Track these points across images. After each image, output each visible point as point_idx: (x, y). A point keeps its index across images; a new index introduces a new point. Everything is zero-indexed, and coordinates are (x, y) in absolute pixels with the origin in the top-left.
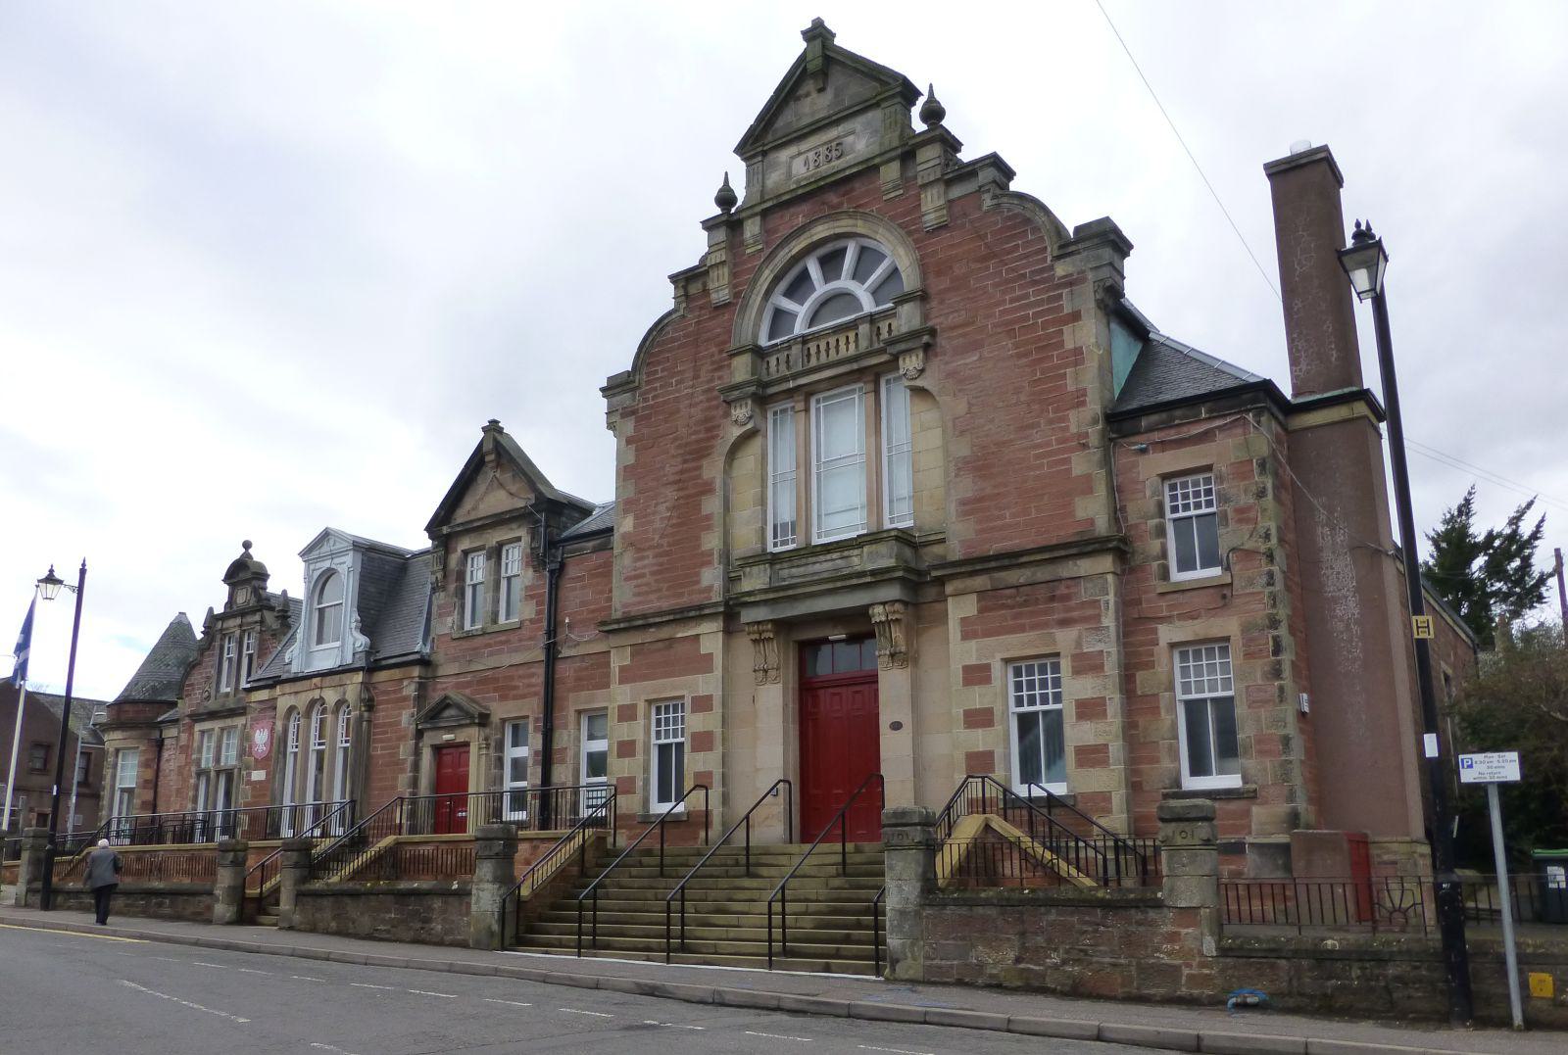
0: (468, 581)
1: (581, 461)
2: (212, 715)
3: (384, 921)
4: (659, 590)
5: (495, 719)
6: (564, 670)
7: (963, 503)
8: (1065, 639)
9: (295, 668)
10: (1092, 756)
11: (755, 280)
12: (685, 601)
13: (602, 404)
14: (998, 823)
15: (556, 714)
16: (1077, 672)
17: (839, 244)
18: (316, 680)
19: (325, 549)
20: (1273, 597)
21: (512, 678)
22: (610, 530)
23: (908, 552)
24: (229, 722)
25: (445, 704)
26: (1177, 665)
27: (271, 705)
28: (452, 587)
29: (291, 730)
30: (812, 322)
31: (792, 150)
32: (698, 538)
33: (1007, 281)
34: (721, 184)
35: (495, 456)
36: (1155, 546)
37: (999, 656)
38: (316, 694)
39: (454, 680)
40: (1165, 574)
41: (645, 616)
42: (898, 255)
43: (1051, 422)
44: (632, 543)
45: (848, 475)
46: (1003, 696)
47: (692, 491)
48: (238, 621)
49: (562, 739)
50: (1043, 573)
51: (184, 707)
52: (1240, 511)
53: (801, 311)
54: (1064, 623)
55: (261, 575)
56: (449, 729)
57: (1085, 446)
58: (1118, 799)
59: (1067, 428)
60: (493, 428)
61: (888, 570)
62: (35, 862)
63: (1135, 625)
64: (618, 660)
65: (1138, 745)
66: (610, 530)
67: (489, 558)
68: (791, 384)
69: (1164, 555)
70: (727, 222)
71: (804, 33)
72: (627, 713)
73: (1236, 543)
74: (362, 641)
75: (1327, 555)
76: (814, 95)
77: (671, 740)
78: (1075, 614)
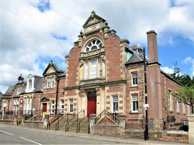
0: (48, 81)
1: (63, 66)
4: (71, 84)
8: (119, 93)
10: (121, 108)
12: (73, 86)
14: (107, 116)
27: (23, 97)
32: (76, 78)
38: (28, 96)
40: (131, 85)
45: (91, 71)
46: (112, 100)
51: (13, 96)
53: (90, 48)
54: (119, 91)
63: (128, 91)
64: (66, 93)
65: (128, 107)
69: (131, 82)
78: (120, 90)
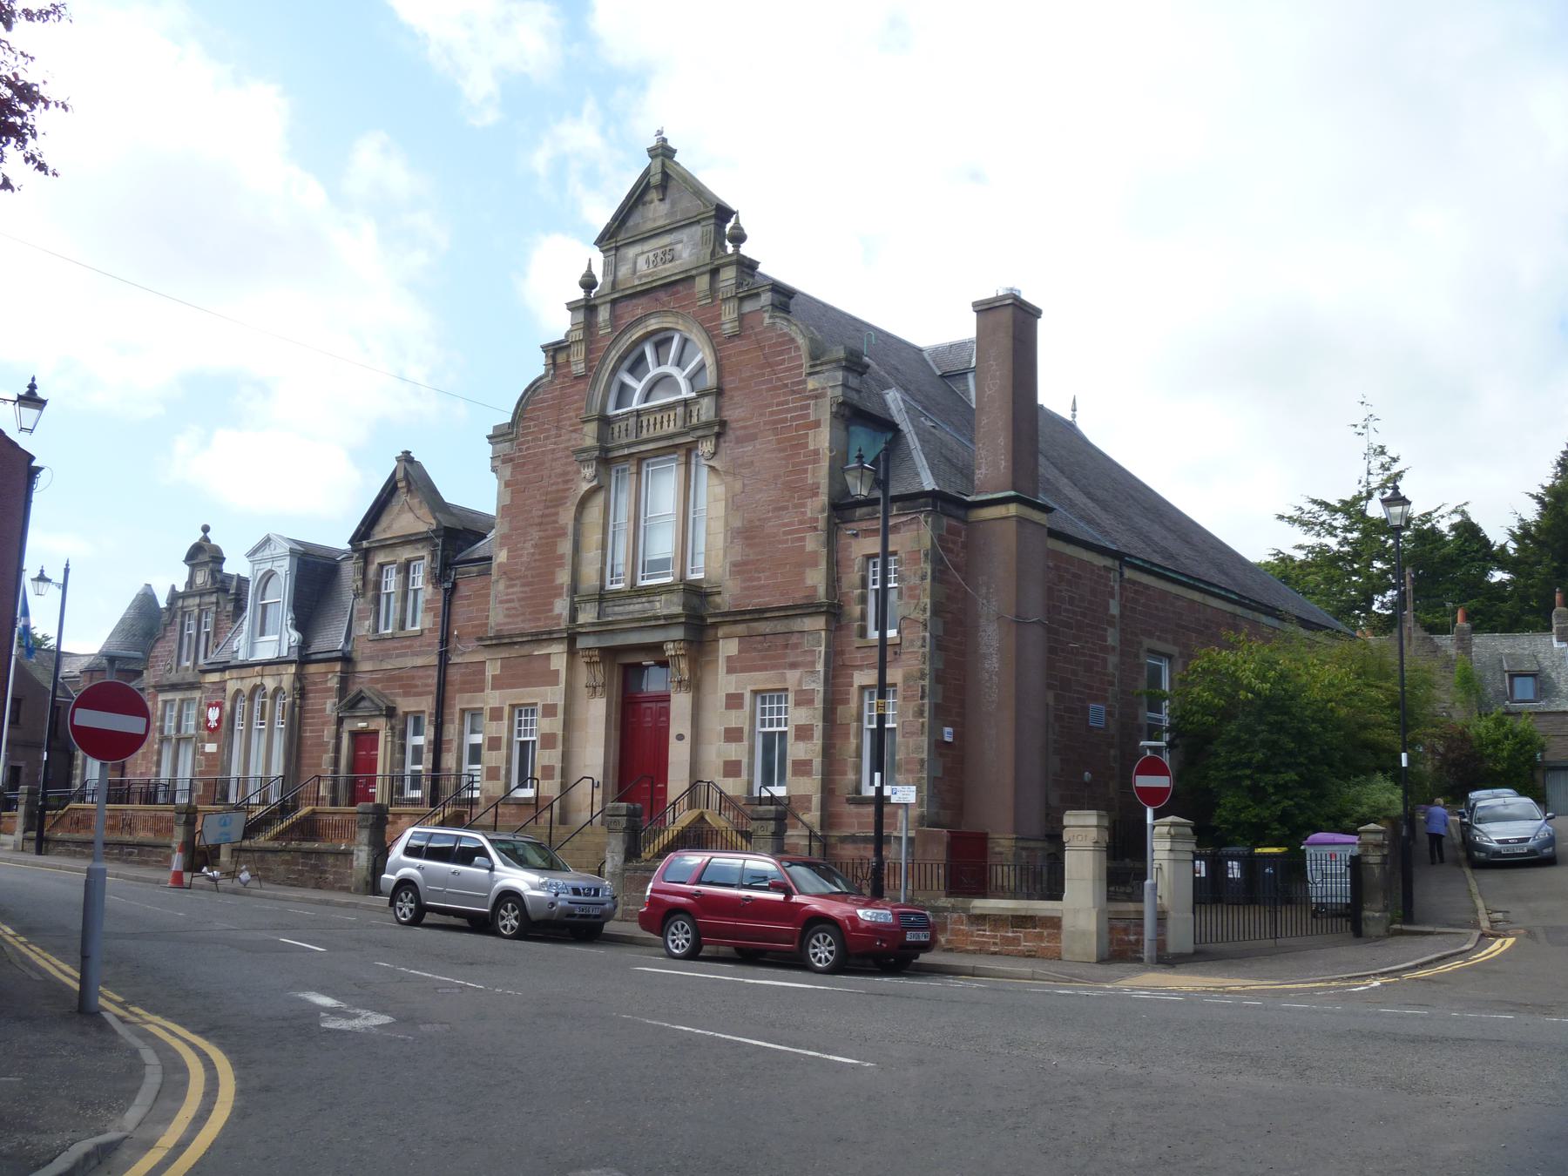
2: (174, 687)
3: (294, 872)
5: (400, 711)
6: (454, 674)
7: (734, 565)
8: (792, 677)
9: (241, 656)
10: (802, 767)
11: (605, 358)
13: (488, 449)
15: (447, 711)
16: (798, 704)
17: (669, 334)
18: (258, 668)
19: (267, 553)
20: (924, 655)
21: (413, 678)
22: (490, 558)
23: (695, 601)
24: (188, 694)
25: (360, 698)
26: (759, 706)
28: (370, 594)
29: (238, 710)
30: (646, 399)
31: (636, 249)
32: (553, 573)
33: (776, 388)
34: (584, 270)
35: (407, 480)
36: (856, 610)
37: (750, 688)
38: (258, 681)
39: (368, 676)
41: (510, 636)
42: (703, 354)
43: (795, 506)
44: (506, 572)
45: (673, 525)
47: (550, 532)
48: (197, 600)
49: (451, 731)
50: (780, 626)
52: (911, 589)
53: (639, 387)
54: (793, 666)
55: (218, 558)
56: (363, 718)
57: (816, 529)
58: (816, 800)
59: (804, 513)
60: (407, 458)
61: (677, 616)
62: (29, 816)
63: (836, 672)
64: (492, 669)
66: (490, 558)
67: (398, 572)
68: (626, 452)
69: (863, 617)
70: (586, 309)
71: (649, 150)
72: (496, 714)
73: (906, 613)
74: (295, 636)
75: (983, 622)
76: (657, 202)
77: (775, 729)
